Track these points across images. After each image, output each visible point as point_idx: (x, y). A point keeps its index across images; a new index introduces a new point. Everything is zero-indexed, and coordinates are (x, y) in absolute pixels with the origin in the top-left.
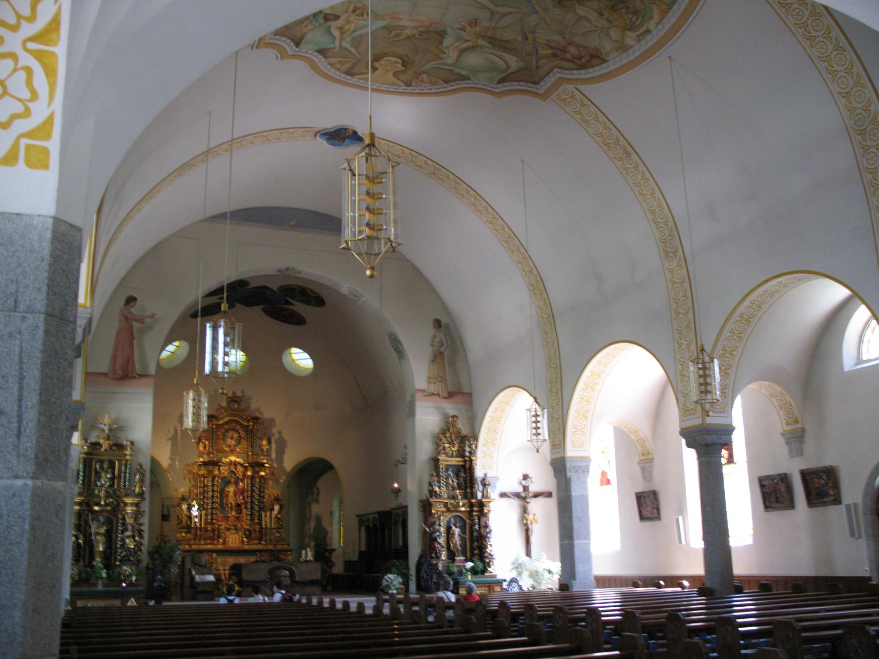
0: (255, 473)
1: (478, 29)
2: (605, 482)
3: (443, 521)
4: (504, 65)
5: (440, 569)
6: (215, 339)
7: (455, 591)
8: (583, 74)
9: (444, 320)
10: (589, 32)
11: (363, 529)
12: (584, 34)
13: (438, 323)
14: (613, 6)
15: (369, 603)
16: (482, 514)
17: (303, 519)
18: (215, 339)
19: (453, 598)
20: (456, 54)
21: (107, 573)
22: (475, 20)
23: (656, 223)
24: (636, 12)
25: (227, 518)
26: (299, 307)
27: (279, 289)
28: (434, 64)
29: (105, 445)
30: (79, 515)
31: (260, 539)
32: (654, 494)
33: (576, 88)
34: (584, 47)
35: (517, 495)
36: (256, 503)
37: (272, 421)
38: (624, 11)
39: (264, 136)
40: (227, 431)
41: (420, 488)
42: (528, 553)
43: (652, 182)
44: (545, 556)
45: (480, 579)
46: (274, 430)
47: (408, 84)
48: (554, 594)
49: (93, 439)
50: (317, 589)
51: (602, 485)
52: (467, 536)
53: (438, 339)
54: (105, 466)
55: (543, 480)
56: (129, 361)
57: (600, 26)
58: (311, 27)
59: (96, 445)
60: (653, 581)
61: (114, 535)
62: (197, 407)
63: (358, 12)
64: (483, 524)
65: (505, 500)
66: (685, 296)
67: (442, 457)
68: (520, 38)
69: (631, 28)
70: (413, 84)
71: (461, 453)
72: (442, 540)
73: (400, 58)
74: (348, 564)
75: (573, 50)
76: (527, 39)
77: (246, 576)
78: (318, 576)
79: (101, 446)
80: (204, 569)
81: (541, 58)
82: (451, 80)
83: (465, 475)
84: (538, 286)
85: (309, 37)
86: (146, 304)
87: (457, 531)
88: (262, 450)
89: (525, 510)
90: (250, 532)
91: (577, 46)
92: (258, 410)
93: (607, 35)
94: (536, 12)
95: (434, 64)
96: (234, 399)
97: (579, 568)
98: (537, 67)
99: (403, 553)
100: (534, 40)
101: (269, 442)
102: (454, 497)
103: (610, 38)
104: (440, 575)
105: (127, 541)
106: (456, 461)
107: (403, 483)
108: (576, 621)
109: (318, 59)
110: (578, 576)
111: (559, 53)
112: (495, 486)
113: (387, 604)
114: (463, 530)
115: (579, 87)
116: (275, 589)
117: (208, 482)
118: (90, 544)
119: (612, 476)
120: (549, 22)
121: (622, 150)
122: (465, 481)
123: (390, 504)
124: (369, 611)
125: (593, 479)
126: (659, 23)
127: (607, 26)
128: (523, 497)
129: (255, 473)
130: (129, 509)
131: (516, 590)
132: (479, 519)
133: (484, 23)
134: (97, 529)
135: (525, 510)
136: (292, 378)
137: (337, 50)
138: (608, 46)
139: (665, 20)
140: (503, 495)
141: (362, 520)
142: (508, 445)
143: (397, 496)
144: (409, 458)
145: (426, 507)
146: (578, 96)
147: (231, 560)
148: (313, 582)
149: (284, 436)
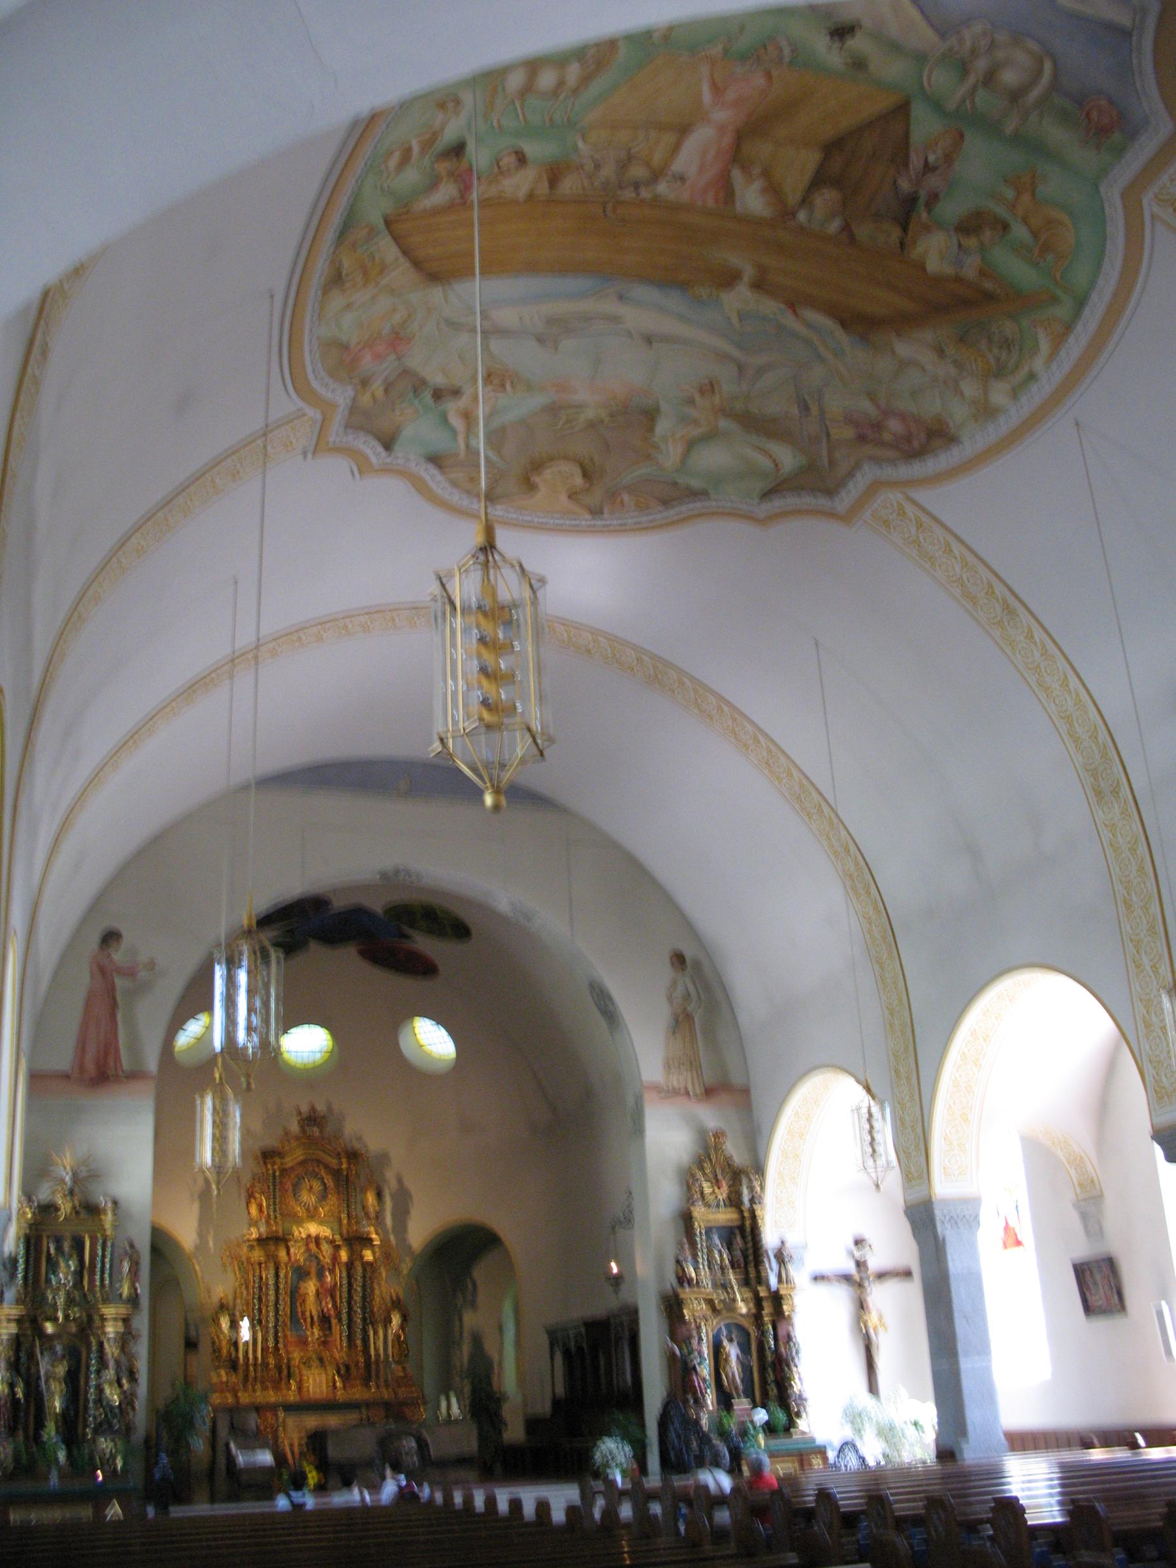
0: (355, 1256)
1: (717, 400)
2: (1011, 1241)
3: (707, 1333)
4: (767, 464)
5: (705, 1428)
6: (231, 982)
7: (734, 1470)
8: (917, 469)
9: (688, 954)
11: (559, 1357)
13: (679, 960)
15: (561, 1497)
16: (779, 1315)
17: (447, 1341)
18: (231, 982)
19: (724, 1481)
21: (70, 1455)
23: (1076, 740)
24: (1007, 344)
25: (303, 1342)
26: (424, 944)
27: (386, 912)
28: (644, 470)
29: (65, 1207)
30: (17, 1342)
31: (366, 1381)
32: (1110, 1265)
33: (909, 499)
35: (847, 1278)
36: (356, 1307)
37: (384, 1159)
39: (340, 624)
40: (300, 1178)
41: (660, 1269)
42: (873, 1388)
43: (1061, 662)
44: (903, 1392)
45: (781, 1443)
46: (390, 1176)
47: (596, 512)
48: (927, 1471)
49: (43, 1194)
50: (471, 1475)
51: (1005, 1246)
52: (754, 1364)
53: (679, 992)
54: (66, 1246)
55: (891, 1246)
56: (109, 1048)
59: (47, 1210)
60: (1122, 1437)
61: (82, 1382)
62: (221, 1125)
64: (781, 1333)
65: (822, 1289)
66: (1141, 869)
67: (699, 1211)
68: (795, 411)
69: (1000, 372)
70: (606, 510)
71: (734, 1201)
72: (705, 1370)
74: (533, 1424)
75: (895, 425)
77: (333, 1452)
78: (470, 1444)
79: (57, 1209)
80: (252, 1440)
82: (673, 499)
83: (745, 1246)
84: (861, 878)
85: (408, 432)
86: (140, 943)
87: (732, 1351)
88: (367, 1214)
89: (861, 1306)
90: (348, 1368)
91: (903, 417)
92: (359, 1139)
95: (644, 470)
96: (312, 1119)
97: (973, 1415)
98: (832, 463)
99: (633, 1399)
101: (379, 1195)
102: (725, 1286)
103: (962, 394)
104: (704, 1439)
105: (108, 1391)
106: (725, 1216)
107: (627, 1261)
108: (972, 1527)
109: (430, 474)
110: (970, 1428)
112: (801, 1259)
113: (439, 1497)
114: (745, 1348)
116: (388, 1472)
117: (269, 1275)
118: (35, 1396)
119: (1026, 1232)
121: (1001, 606)
122: (744, 1253)
123: (601, 1306)
124: (558, 1515)
125: (988, 1237)
127: (953, 371)
128: (856, 1281)
129: (355, 1256)
130: (111, 1329)
131: (852, 1462)
132: (775, 1328)
134: (52, 1371)
135: (861, 1306)
136: (415, 1076)
138: (958, 413)
139: (1063, 353)
140: (818, 1278)
141: (555, 1337)
142: (821, 1184)
143: (616, 1292)
144: (637, 1217)
145: (672, 1307)
146: (910, 509)
147: (312, 1422)
148: (462, 1461)
149: (409, 1183)
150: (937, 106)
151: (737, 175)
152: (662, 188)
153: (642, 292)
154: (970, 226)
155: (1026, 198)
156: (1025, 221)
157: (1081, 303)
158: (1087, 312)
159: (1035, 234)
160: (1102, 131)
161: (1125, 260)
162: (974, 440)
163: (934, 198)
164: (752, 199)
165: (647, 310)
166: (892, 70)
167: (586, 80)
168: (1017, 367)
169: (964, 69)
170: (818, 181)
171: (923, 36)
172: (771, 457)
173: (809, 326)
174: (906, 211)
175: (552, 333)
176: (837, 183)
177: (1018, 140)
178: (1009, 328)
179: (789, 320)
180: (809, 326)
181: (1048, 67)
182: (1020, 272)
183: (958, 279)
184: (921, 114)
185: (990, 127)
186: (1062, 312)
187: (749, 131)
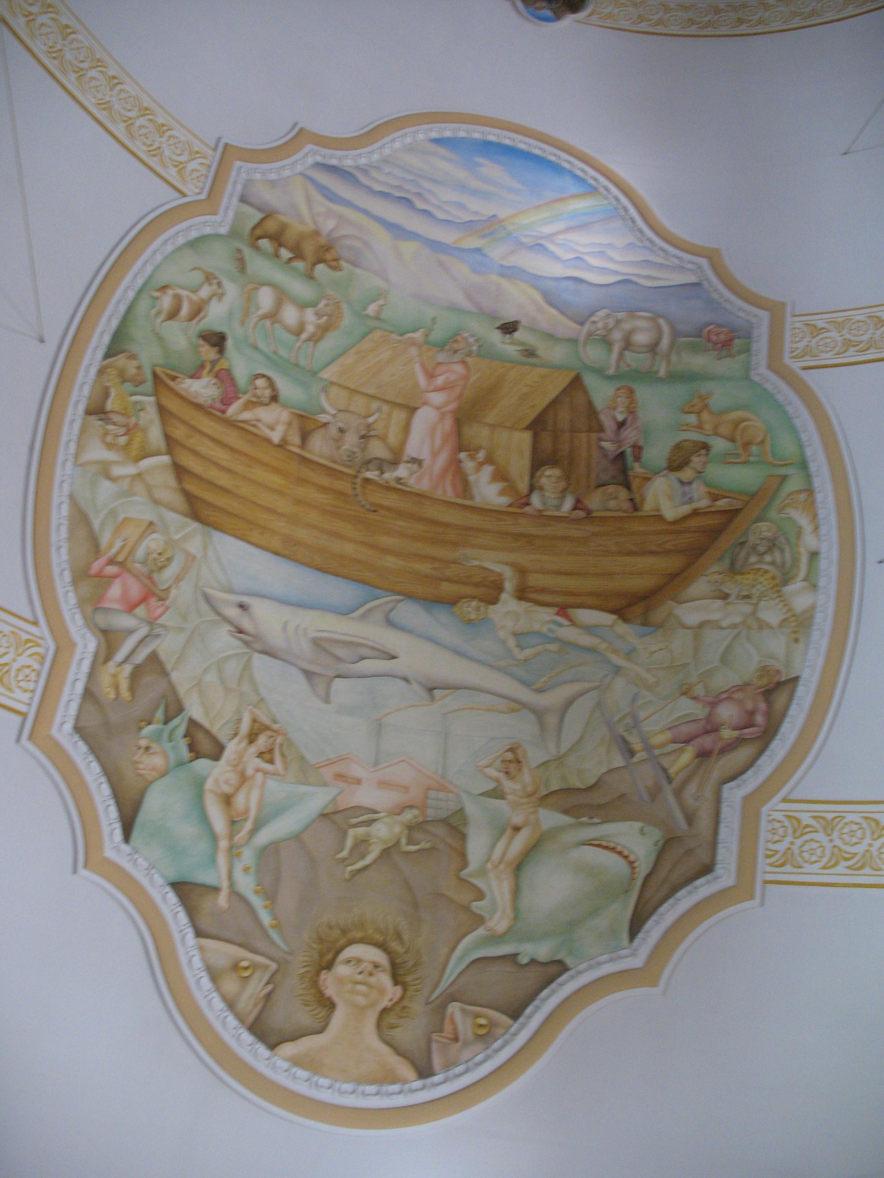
10: (728, 647)
12: (725, 659)
14: (733, 563)
22: (511, 750)
34: (742, 688)
57: (738, 620)
58: (157, 761)
63: (262, 741)
68: (618, 761)
73: (382, 946)
75: (727, 712)
76: (632, 753)
91: (728, 695)
93: (763, 625)
94: (618, 670)
98: (690, 819)
100: (648, 748)
103: (770, 627)
111: (707, 741)
120: (651, 679)
126: (817, 528)
127: (747, 609)
133: (534, 756)
137: (222, 900)
139: (821, 513)
150: (600, 372)
151: (469, 465)
152: (402, 471)
153: (410, 613)
154: (678, 462)
155: (705, 416)
156: (716, 434)
157: (803, 465)
158: (813, 467)
159: (732, 440)
160: (727, 344)
161: (809, 407)
162: (810, 670)
163: (637, 449)
164: (488, 491)
165: (420, 642)
166: (557, 354)
167: (324, 330)
168: (796, 560)
169: (606, 341)
170: (538, 463)
171: (567, 327)
172: (620, 853)
173: (589, 629)
174: (622, 470)
175: (325, 665)
176: (553, 461)
177: (673, 377)
178: (764, 529)
179: (569, 633)
180: (589, 629)
181: (661, 321)
182: (741, 477)
183: (695, 513)
184: (591, 381)
185: (648, 376)
186: (794, 484)
187: (465, 415)
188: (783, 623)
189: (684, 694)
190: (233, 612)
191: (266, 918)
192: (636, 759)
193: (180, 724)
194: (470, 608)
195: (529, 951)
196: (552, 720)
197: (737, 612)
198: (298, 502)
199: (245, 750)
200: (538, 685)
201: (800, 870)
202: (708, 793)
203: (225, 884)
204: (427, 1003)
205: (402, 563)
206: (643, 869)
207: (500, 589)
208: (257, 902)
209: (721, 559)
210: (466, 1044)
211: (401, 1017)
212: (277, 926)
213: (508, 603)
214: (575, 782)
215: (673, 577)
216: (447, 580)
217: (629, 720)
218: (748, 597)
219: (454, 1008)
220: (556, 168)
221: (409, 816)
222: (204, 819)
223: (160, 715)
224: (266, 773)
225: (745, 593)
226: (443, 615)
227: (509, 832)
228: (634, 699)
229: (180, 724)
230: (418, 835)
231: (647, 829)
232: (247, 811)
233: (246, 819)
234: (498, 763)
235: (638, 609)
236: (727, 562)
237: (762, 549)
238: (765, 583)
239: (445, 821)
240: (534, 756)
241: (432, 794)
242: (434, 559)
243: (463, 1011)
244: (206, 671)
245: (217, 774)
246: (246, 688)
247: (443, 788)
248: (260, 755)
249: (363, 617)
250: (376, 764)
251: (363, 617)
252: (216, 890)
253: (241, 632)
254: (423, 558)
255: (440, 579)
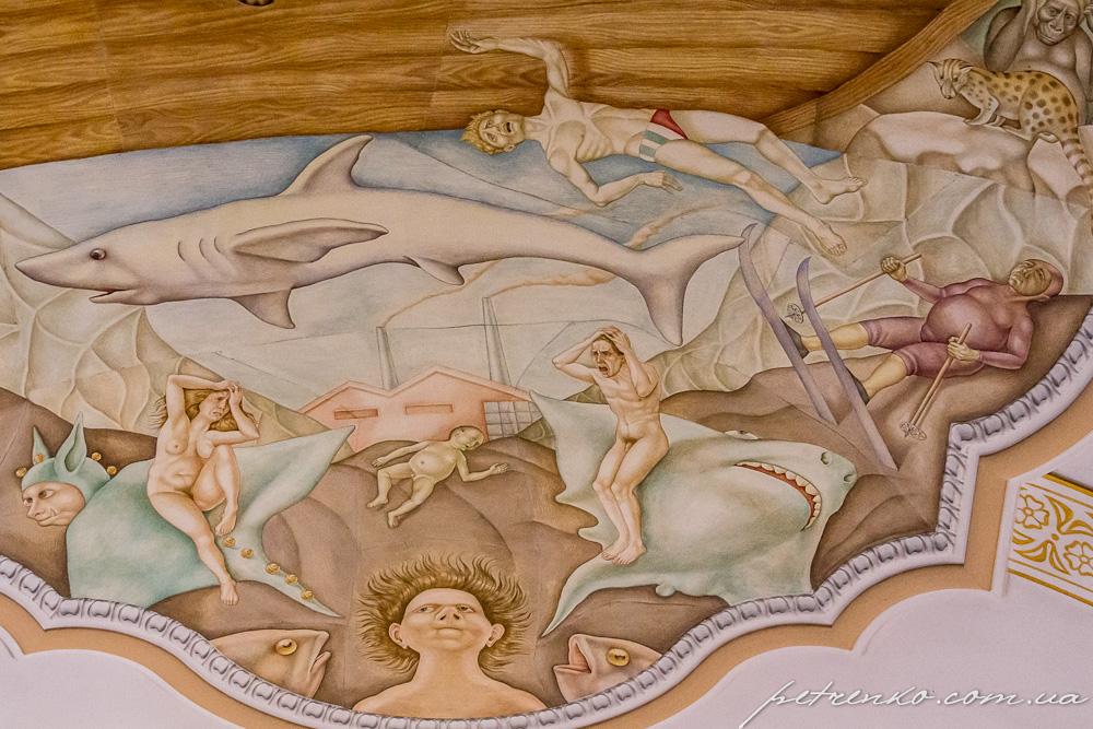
14: (990, 48)
20: (628, 508)
34: (992, 285)
38: (1032, 50)
57: (993, 163)
58: (67, 499)
63: (209, 409)
68: (780, 358)
73: (465, 587)
76: (803, 351)
81: (890, 406)
91: (968, 290)
93: (1035, 186)
94: (771, 219)
100: (828, 345)
111: (928, 354)
115: (1058, 463)
120: (831, 240)
127: (1014, 148)
137: (228, 593)
153: (385, 159)
172: (793, 482)
173: (714, 148)
179: (677, 154)
180: (714, 148)
188: (1076, 193)
189: (891, 272)
190: (88, 272)
191: (296, 593)
192: (807, 360)
193: (75, 445)
194: (494, 130)
195: (668, 583)
196: (666, 294)
197: (992, 149)
198: (118, 46)
199: (187, 431)
200: (636, 240)
201: (1063, 575)
202: (929, 428)
203: (224, 579)
204: (540, 637)
205: (348, 78)
206: (828, 507)
207: (545, 86)
208: (277, 581)
209: (967, 34)
210: (600, 674)
211: (508, 654)
212: (315, 595)
213: (561, 109)
214: (712, 382)
215: (871, 58)
216: (439, 89)
217: (795, 300)
218: (1018, 125)
219: (579, 641)
220: (356, 60)
221: (463, 439)
222: (165, 525)
223: (39, 448)
224: (229, 444)
225: (1010, 115)
226: (446, 149)
227: (619, 444)
228: (803, 268)
229: (75, 445)
230: (481, 460)
231: (829, 456)
232: (222, 493)
233: (225, 502)
234: (586, 357)
235: (806, 113)
236: (980, 41)
237: (1052, 33)
238: (1050, 106)
239: (520, 437)
240: (644, 345)
241: (493, 406)
242: (407, 55)
243: (590, 642)
244: (81, 364)
245: (161, 473)
246: (154, 355)
247: (508, 397)
248: (213, 426)
249: (308, 187)
250: (393, 386)
251: (308, 187)
252: (217, 587)
253: (110, 291)
254: (385, 58)
255: (430, 89)
